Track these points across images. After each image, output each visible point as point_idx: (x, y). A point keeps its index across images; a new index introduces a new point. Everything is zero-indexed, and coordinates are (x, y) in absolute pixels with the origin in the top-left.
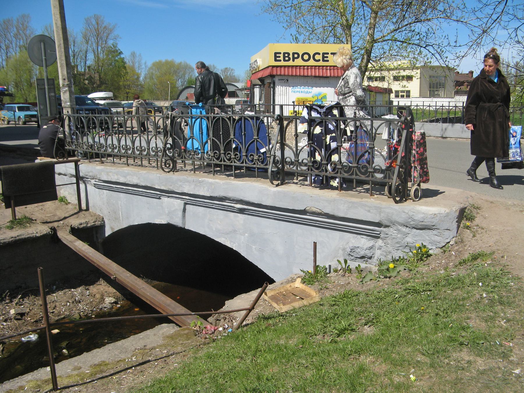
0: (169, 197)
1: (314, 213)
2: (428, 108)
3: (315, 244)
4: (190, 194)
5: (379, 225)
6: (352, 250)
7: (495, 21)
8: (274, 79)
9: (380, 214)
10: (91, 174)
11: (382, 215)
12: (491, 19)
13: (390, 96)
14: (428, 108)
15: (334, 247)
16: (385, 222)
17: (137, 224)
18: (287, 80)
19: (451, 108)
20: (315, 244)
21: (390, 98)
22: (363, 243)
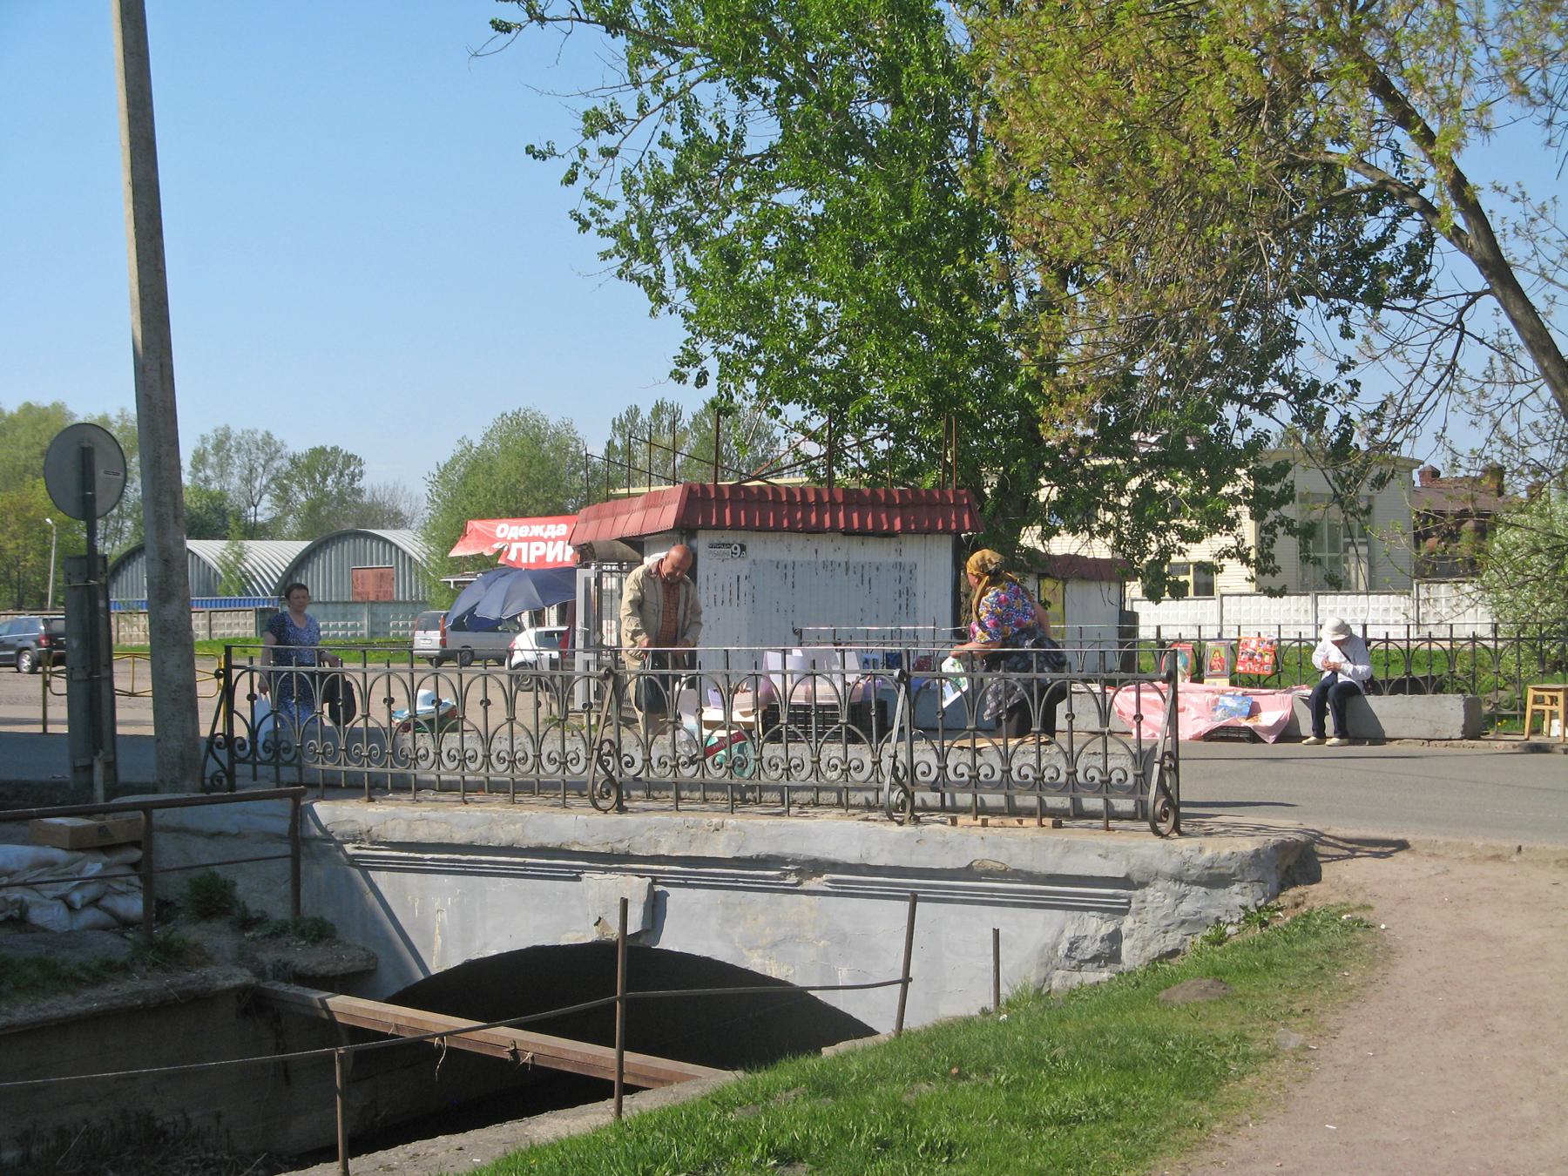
0: (606, 871)
1: (990, 874)
2: (1426, 646)
3: (996, 932)
4: (677, 857)
5: (1126, 882)
6: (1073, 946)
7: (1436, 386)
8: (694, 543)
9: (1128, 859)
10: (348, 828)
11: (1132, 861)
12: (1419, 381)
13: (1122, 594)
14: (1426, 646)
15: (1032, 934)
16: (1136, 877)
17: (494, 952)
18: (743, 548)
19: (1413, 645)
20: (996, 932)
21: (1122, 602)
22: (1095, 927)
